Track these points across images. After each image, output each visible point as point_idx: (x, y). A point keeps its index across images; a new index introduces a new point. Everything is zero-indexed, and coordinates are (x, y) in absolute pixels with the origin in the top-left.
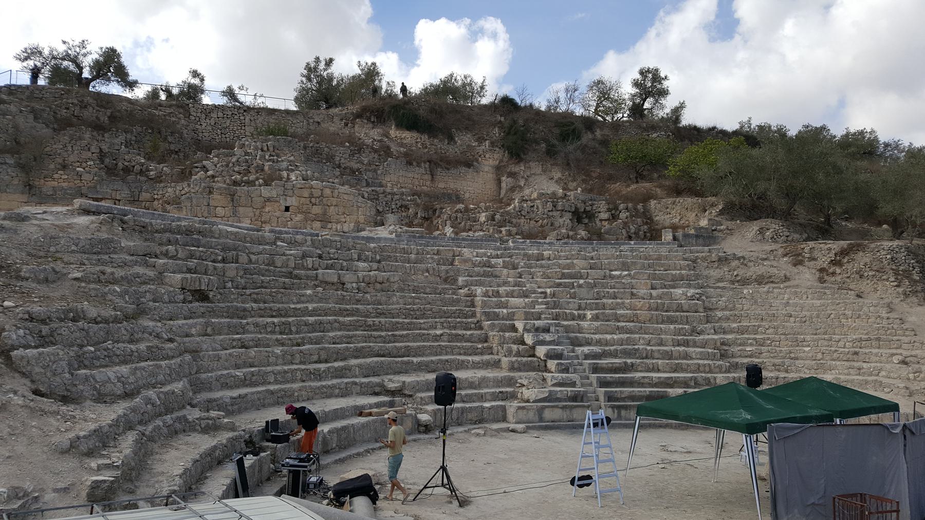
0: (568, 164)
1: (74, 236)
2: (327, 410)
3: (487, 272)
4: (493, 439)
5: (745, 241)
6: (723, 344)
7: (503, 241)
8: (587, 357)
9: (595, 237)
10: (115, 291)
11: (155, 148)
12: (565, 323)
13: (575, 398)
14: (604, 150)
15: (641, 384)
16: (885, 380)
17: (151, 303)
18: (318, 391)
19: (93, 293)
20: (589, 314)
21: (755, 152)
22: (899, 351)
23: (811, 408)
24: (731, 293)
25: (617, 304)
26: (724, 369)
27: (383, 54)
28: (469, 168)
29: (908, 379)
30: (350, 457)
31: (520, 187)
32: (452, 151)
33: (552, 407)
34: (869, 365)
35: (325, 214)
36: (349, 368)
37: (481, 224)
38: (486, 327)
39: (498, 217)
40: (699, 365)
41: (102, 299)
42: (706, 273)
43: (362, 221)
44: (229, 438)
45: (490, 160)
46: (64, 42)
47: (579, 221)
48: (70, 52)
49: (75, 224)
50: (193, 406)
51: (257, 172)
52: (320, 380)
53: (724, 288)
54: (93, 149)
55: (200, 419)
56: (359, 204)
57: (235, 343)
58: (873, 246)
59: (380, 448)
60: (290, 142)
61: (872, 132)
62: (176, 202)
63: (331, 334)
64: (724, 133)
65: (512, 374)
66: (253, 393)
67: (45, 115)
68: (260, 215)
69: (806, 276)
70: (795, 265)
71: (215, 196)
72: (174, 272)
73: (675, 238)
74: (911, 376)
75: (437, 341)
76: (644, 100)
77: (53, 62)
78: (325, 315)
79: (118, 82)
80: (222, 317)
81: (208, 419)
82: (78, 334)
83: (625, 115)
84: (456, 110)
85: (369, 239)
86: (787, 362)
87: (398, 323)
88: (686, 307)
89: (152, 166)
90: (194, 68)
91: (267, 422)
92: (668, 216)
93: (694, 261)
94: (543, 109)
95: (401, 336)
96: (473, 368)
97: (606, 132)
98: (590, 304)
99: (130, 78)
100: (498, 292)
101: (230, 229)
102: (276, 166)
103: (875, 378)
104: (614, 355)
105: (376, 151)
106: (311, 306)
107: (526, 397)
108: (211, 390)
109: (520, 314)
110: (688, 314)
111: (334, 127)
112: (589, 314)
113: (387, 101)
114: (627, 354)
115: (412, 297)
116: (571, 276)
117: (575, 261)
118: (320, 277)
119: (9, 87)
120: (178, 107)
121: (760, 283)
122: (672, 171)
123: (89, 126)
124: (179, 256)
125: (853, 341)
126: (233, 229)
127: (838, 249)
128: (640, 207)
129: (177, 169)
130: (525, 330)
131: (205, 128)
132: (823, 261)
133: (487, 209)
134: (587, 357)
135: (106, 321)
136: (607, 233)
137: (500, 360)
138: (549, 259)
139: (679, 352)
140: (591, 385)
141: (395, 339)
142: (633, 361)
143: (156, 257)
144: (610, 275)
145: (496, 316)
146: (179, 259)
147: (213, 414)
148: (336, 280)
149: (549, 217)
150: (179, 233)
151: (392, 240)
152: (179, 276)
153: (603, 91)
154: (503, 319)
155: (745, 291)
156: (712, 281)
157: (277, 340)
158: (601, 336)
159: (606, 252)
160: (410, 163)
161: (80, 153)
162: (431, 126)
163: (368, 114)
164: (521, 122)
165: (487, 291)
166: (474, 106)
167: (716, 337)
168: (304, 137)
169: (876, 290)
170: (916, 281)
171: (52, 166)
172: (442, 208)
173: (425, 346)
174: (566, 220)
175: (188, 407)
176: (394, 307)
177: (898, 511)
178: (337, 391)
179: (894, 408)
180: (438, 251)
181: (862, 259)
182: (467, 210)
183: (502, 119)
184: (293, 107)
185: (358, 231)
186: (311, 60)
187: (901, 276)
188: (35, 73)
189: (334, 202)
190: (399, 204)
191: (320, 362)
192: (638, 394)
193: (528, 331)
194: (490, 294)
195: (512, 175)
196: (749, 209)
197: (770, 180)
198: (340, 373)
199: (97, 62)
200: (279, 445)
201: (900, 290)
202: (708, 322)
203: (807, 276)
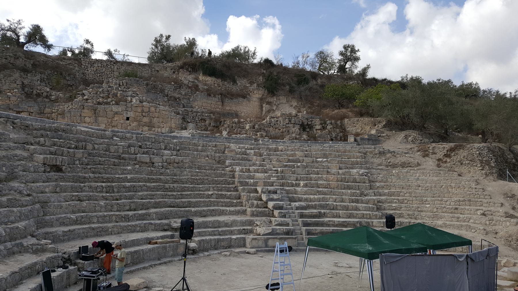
0: (301, 98)
2: (127, 240)
3: (244, 157)
4: (235, 258)
5: (397, 143)
6: (379, 202)
7: (256, 140)
8: (297, 208)
9: (312, 139)
11: (58, 83)
12: (287, 188)
13: (288, 233)
14: (322, 90)
15: (329, 225)
16: (472, 225)
17: (21, 173)
21: (404, 92)
22: (481, 208)
23: (413, 243)
24: (385, 172)
25: (319, 178)
26: (378, 217)
27: (209, 35)
28: (244, 98)
29: (486, 224)
30: (138, 270)
31: (273, 110)
32: (235, 89)
33: (274, 238)
34: (463, 216)
35: (150, 122)
36: (149, 215)
37: (246, 131)
38: (240, 190)
39: (256, 126)
40: (363, 214)
42: (372, 160)
43: (174, 127)
44: (49, 257)
45: (257, 94)
46: (8, 21)
47: (304, 130)
48: (12, 26)
50: (33, 236)
51: (113, 97)
52: (129, 222)
53: (382, 169)
54: (18, 82)
55: (32, 245)
56: (172, 117)
57: (74, 198)
58: (468, 146)
59: (160, 264)
60: (138, 81)
61: (477, 84)
62: (62, 114)
63: (140, 194)
64: (391, 82)
65: (252, 218)
66: (79, 229)
68: (111, 122)
69: (430, 163)
70: (424, 157)
71: (85, 111)
72: (41, 154)
74: (488, 222)
75: (209, 198)
76: (346, 63)
78: (139, 182)
79: (41, 45)
80: (69, 182)
81: (38, 245)
83: (336, 71)
84: (238, 66)
85: (175, 137)
86: (416, 213)
88: (358, 180)
89: (54, 93)
90: (87, 38)
91: (80, 248)
92: (355, 128)
94: (290, 67)
95: (186, 195)
97: (324, 80)
98: (303, 177)
99: (49, 43)
100: (249, 169)
101: (83, 129)
103: (466, 223)
104: (314, 207)
105: (190, 87)
106: (129, 177)
107: (258, 232)
108: (52, 226)
109: (261, 183)
110: (359, 184)
111: (166, 74)
112: (302, 183)
115: (196, 172)
116: (293, 161)
117: (296, 152)
118: (138, 159)
120: (75, 60)
121: (403, 167)
122: (357, 102)
124: (46, 144)
127: (448, 148)
128: (339, 122)
129: (68, 95)
130: (262, 192)
131: (90, 73)
132: (440, 155)
133: (251, 122)
134: (297, 208)
136: (319, 137)
137: (246, 210)
138: (282, 151)
139: (352, 206)
140: (298, 225)
141: (182, 197)
142: (325, 211)
143: (32, 144)
144: (316, 161)
145: (247, 184)
146: (46, 146)
147: (43, 242)
148: (148, 161)
149: (286, 127)
150: (50, 131)
151: (189, 138)
152: (42, 156)
153: (323, 57)
154: (251, 185)
155: (394, 172)
156: (375, 165)
157: (103, 197)
158: (308, 196)
159: (315, 148)
160: (209, 95)
164: (275, 74)
165: (242, 169)
166: (249, 64)
167: (374, 198)
169: (470, 172)
170: (492, 167)
172: (225, 121)
174: (296, 129)
175: (29, 237)
176: (184, 177)
178: (139, 228)
179: (469, 243)
180: (216, 145)
181: (462, 153)
182: (239, 122)
184: (145, 61)
185: (171, 133)
186: (158, 35)
187: (484, 164)
191: (131, 210)
192: (325, 231)
193: (264, 193)
194: (244, 170)
195: (269, 103)
196: (399, 124)
197: (412, 108)
198: (142, 217)
200: (86, 262)
201: (484, 172)
202: (371, 189)
203: (431, 163)
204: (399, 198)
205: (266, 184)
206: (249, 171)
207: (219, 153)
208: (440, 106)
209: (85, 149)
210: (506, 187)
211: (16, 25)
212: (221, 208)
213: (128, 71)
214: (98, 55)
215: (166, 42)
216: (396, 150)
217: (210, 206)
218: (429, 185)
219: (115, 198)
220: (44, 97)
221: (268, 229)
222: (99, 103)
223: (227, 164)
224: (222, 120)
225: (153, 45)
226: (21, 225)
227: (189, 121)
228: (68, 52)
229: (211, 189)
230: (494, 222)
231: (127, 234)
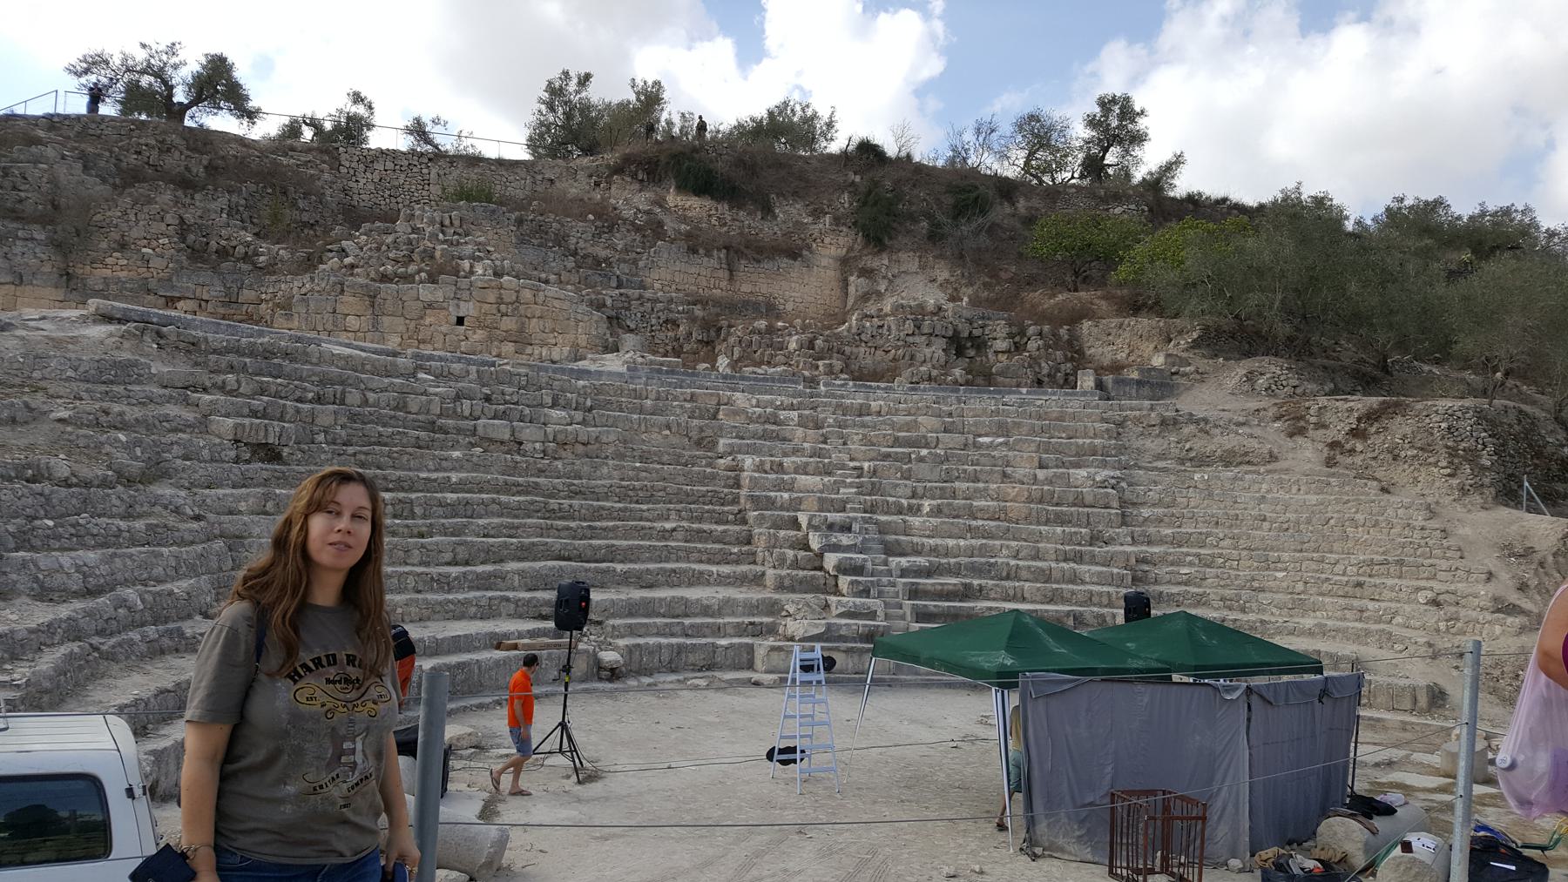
0: (962, 257)
1: (73, 356)
2: (440, 636)
3: (770, 431)
4: (719, 694)
5: (1223, 395)
6: (1144, 561)
9: (980, 380)
10: (117, 440)
17: (179, 461)
18: (438, 608)
19: (82, 442)
20: (927, 505)
24: (1173, 478)
25: (976, 490)
29: (1438, 630)
31: (879, 295)
32: (768, 230)
34: (1377, 605)
35: (521, 331)
36: (503, 577)
37: (789, 356)
38: (751, 521)
39: (819, 342)
40: (1091, 592)
41: (94, 452)
42: (1137, 444)
45: (831, 247)
46: (144, 46)
47: (960, 353)
49: (84, 336)
52: (449, 592)
54: (169, 218)
58: (1419, 406)
60: (494, 211)
61: (1527, 211)
62: (286, 306)
63: (481, 522)
64: (1240, 208)
65: (777, 596)
67: (102, 164)
69: (1306, 454)
70: (1291, 435)
71: (347, 298)
72: (227, 415)
73: (1100, 385)
74: (1442, 625)
76: (1106, 150)
77: (126, 77)
78: (480, 492)
82: (30, 500)
84: (779, 163)
87: (603, 508)
88: (1089, 499)
89: (264, 247)
93: (1120, 424)
94: (940, 163)
96: (719, 585)
97: (1036, 202)
100: (781, 464)
101: (337, 350)
102: (455, 251)
103: (1382, 626)
104: (955, 571)
105: (638, 229)
109: (811, 502)
111: (575, 189)
113: (665, 146)
114: (977, 570)
115: (634, 468)
118: (480, 431)
119: (49, 118)
121: (1227, 464)
123: (172, 181)
125: (1360, 565)
126: (348, 351)
127: (1364, 411)
128: (1063, 331)
129: (301, 254)
130: (810, 525)
131: (364, 188)
132: (1338, 429)
134: (904, 573)
135: (87, 484)
137: (763, 574)
138: (879, 413)
139: (1063, 570)
140: (903, 617)
141: (594, 533)
142: (983, 582)
143: (205, 390)
145: (771, 504)
146: (242, 395)
148: (507, 437)
149: (907, 345)
150: (252, 354)
151: (621, 375)
152: (230, 421)
153: (1038, 134)
154: (782, 508)
156: (1147, 457)
158: (939, 541)
159: (980, 405)
161: (149, 229)
162: (734, 188)
163: (633, 168)
167: (1129, 549)
168: (520, 206)
169: (1416, 481)
171: (104, 245)
172: (730, 326)
173: (639, 547)
175: (198, 618)
177: (1204, 819)
180: (692, 395)
181: (1401, 427)
182: (771, 330)
183: (858, 179)
184: (521, 154)
186: (555, 74)
188: (96, 95)
189: (538, 310)
190: (663, 318)
194: (767, 467)
195: (867, 273)
196: (1235, 339)
198: (484, 582)
199: (198, 78)
201: (1455, 482)
202: (1124, 523)
203: (1308, 454)
204: (1202, 551)
205: (824, 505)
206: (780, 468)
207: (701, 417)
208: (1353, 287)
209: (343, 402)
210: (1514, 527)
211: (164, 57)
212: (694, 566)
213: (468, 181)
214: (386, 136)
215: (577, 92)
216: (1212, 414)
217: (667, 561)
218: (1291, 516)
219: (415, 531)
220: (238, 260)
221: (816, 626)
222: (384, 278)
223: (721, 448)
224: (724, 323)
225: (544, 102)
226: (180, 587)
227: (633, 326)
228: (304, 128)
229: (673, 515)
230: (1459, 625)
231: (443, 623)
